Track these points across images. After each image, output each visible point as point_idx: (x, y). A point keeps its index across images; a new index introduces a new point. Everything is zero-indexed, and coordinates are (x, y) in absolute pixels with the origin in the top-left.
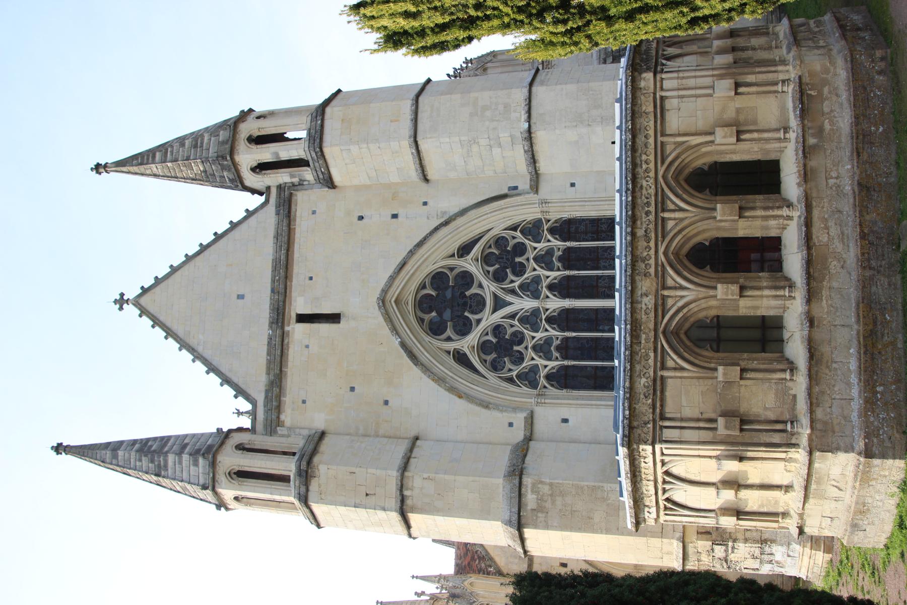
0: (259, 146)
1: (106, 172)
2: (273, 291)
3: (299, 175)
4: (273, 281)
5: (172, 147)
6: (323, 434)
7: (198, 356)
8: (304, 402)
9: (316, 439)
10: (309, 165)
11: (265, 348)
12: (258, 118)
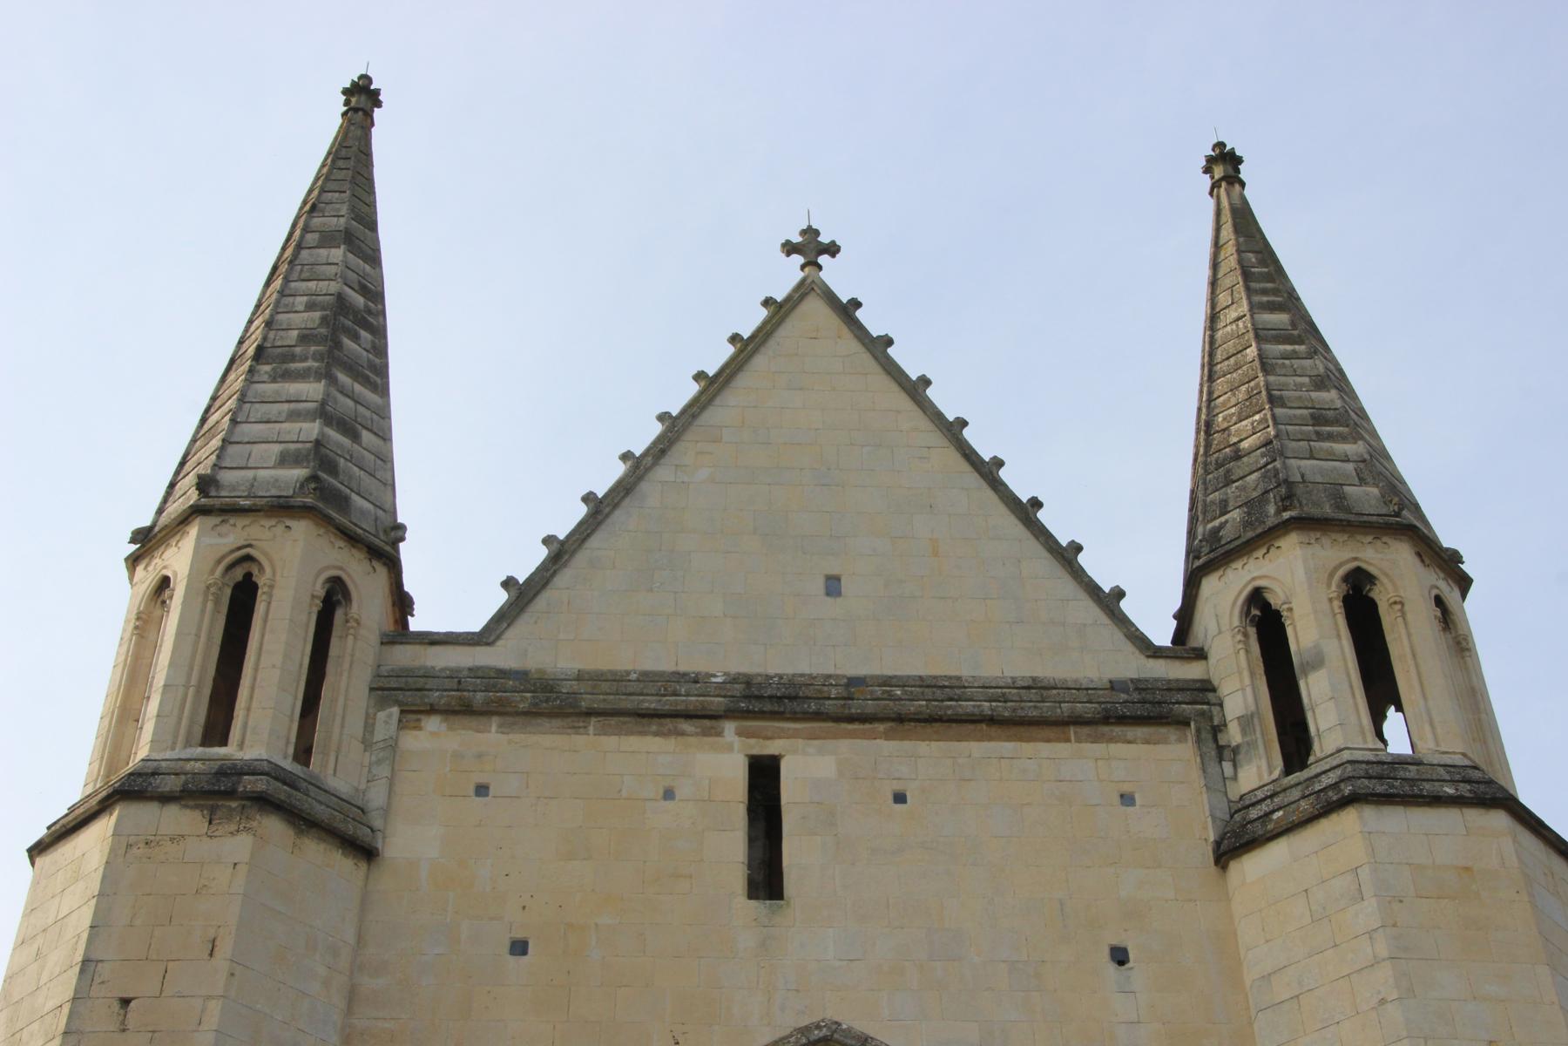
0: (1337, 604)
1: (1215, 186)
2: (854, 682)
3: (1251, 745)
4: (887, 681)
5: (1312, 354)
6: (366, 852)
7: (639, 468)
8: (482, 790)
9: (350, 829)
10: (1288, 770)
11: (667, 666)
12: (1439, 601)
